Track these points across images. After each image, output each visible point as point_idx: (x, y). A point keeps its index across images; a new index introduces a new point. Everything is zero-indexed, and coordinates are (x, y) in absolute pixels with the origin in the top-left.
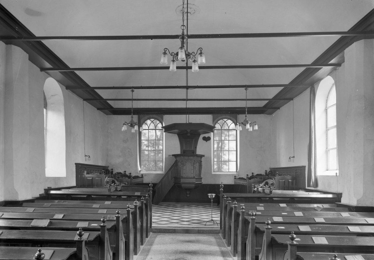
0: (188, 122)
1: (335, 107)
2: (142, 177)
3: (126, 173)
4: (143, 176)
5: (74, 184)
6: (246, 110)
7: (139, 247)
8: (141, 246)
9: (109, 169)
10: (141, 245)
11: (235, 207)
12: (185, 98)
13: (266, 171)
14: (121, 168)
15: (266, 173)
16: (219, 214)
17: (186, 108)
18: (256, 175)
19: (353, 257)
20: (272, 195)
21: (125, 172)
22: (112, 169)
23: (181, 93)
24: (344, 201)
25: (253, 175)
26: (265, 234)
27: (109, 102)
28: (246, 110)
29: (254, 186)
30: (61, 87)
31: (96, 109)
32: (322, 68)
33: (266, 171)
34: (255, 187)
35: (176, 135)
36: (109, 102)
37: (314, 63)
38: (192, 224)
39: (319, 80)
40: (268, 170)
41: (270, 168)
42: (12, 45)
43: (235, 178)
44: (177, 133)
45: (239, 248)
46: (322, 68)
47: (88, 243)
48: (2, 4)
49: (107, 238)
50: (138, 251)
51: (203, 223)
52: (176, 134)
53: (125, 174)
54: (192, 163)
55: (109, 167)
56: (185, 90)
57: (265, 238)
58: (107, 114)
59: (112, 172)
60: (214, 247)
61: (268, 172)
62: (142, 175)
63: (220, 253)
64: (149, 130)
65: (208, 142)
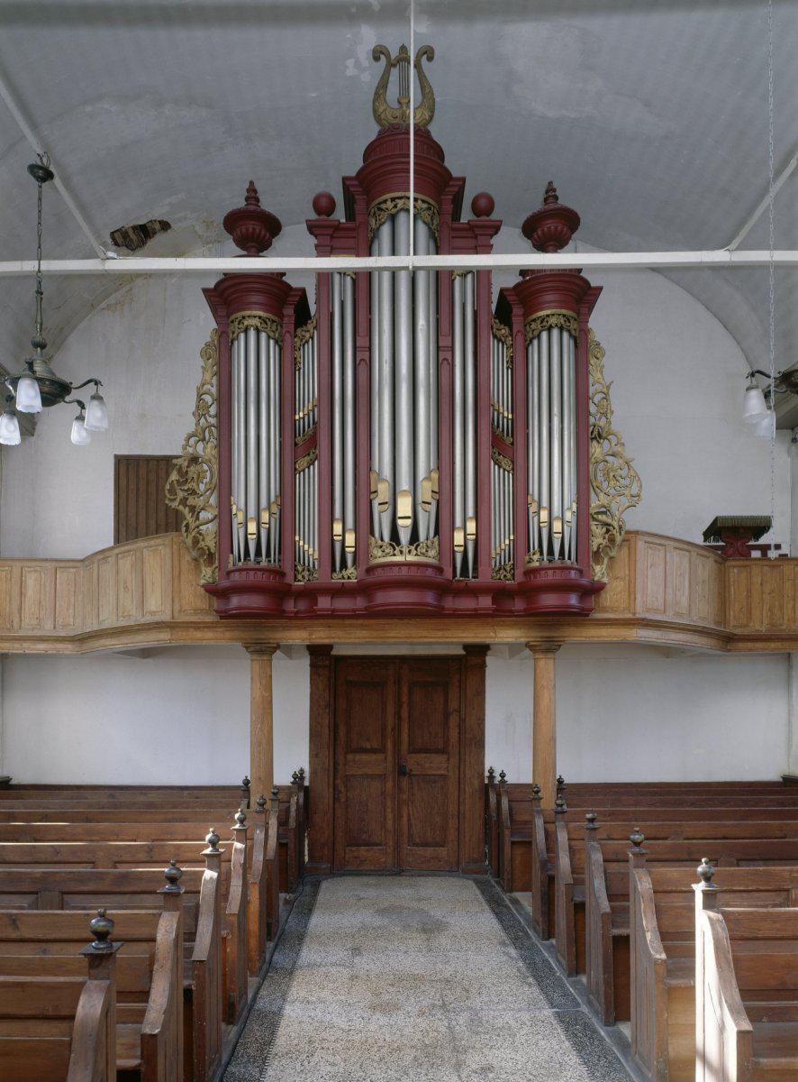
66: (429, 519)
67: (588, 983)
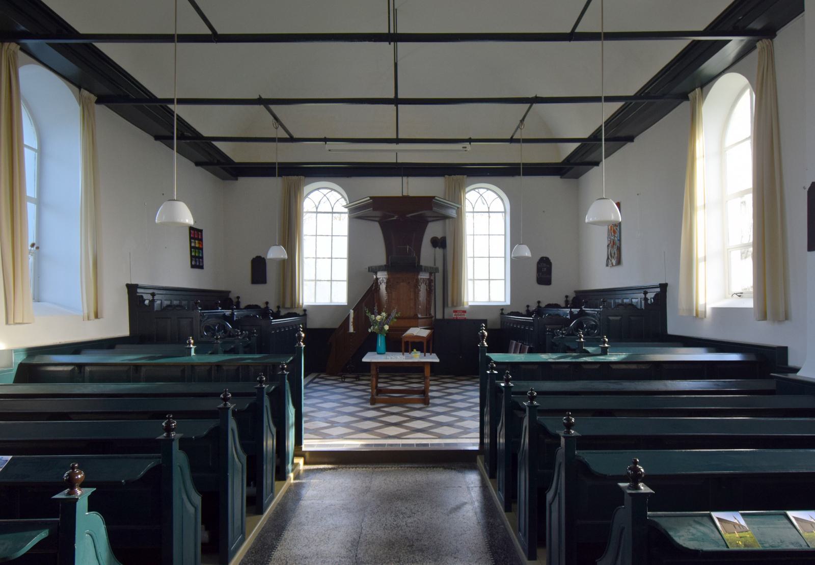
0: (405, 179)
3: (269, 306)
4: (307, 313)
5: (125, 331)
6: (521, 167)
9: (233, 296)
11: (532, 407)
13: (567, 297)
16: (478, 382)
17: (397, 164)
18: (545, 307)
19: (378, 217)
21: (267, 303)
22: (238, 298)
25: (539, 307)
27: (217, 144)
28: (521, 167)
30: (68, 86)
31: (193, 164)
32: (729, 41)
33: (567, 297)
36: (218, 144)
37: (709, 31)
39: (708, 81)
40: (572, 295)
41: (576, 292)
43: (502, 314)
44: (377, 219)
46: (729, 41)
50: (265, 502)
51: (445, 394)
52: (376, 221)
53: (267, 308)
58: (224, 178)
61: (570, 299)
62: (305, 310)
64: (334, 215)
65: (635, 140)
66: (764, 222)
67: (269, 107)
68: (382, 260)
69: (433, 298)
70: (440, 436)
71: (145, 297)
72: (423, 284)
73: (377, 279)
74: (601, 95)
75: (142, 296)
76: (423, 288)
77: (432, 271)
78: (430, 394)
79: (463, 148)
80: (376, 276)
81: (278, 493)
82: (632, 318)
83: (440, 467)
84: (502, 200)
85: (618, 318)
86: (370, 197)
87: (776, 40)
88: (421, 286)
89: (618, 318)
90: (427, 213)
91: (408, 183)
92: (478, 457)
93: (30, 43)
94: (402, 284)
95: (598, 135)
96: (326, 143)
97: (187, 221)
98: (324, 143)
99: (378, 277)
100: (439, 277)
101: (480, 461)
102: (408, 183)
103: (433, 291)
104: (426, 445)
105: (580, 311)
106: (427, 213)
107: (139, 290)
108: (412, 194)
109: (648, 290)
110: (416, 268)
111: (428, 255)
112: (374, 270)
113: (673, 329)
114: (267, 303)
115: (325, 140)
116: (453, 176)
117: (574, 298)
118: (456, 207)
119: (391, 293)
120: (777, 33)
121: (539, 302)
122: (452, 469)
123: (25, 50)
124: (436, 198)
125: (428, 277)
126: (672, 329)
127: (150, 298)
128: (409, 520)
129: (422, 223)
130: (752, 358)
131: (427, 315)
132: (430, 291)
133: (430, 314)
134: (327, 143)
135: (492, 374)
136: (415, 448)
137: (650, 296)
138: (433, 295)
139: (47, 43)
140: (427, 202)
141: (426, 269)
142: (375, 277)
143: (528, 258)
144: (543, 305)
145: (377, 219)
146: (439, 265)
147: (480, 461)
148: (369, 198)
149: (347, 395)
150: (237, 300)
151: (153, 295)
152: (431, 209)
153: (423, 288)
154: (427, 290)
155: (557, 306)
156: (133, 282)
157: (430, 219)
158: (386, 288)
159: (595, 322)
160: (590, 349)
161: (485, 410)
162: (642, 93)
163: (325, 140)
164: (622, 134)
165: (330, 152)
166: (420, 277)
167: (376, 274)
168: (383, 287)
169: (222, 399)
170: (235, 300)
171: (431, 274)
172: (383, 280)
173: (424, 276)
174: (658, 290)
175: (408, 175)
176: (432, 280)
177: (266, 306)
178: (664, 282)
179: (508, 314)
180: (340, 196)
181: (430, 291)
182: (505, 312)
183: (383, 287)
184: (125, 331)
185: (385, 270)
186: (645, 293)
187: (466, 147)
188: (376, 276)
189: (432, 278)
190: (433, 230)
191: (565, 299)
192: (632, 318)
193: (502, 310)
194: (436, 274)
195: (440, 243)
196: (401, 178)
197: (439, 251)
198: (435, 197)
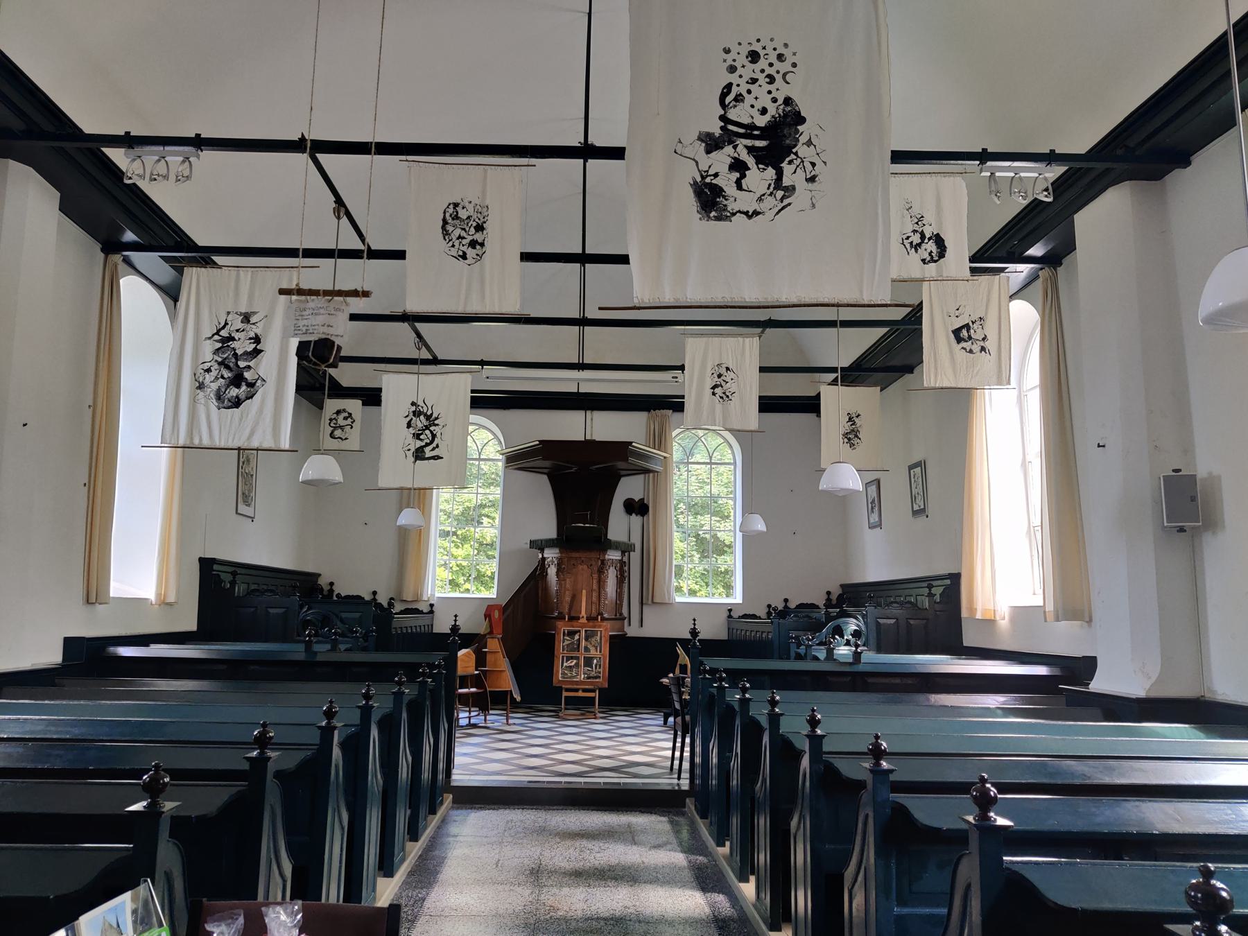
0: (589, 413)
1: (1037, 391)
2: (431, 612)
5: (192, 626)
7: (403, 849)
8: (409, 845)
9: (323, 582)
10: (410, 841)
12: (575, 314)
13: (829, 593)
14: (475, 874)
15: (829, 600)
17: (578, 394)
18: (795, 608)
20: (860, 668)
21: (375, 593)
22: (332, 584)
23: (561, 345)
24: (1098, 685)
25: (786, 607)
26: (865, 796)
29: (797, 638)
30: (162, 297)
33: (829, 593)
34: (799, 645)
35: (545, 477)
38: (591, 772)
40: (836, 592)
41: (842, 586)
42: (11, 161)
43: (730, 616)
44: (546, 471)
45: (763, 858)
47: (180, 825)
48: (2, 49)
49: (272, 807)
50: (396, 860)
53: (375, 599)
54: (596, 569)
55: (320, 575)
56: (597, 140)
57: (867, 811)
59: (331, 591)
60: (668, 852)
61: (834, 597)
63: (687, 875)
68: (551, 532)
69: (626, 590)
70: (636, 776)
71: (223, 576)
72: (611, 568)
73: (544, 559)
74: (841, 329)
75: (218, 575)
76: (611, 576)
77: (626, 549)
78: (647, 475)
79: (673, 377)
80: (543, 555)
81: (409, 855)
82: (912, 622)
83: (636, 811)
84: (731, 447)
85: (892, 621)
86: (539, 441)
87: (1060, 269)
88: (609, 571)
89: (892, 621)
90: (621, 465)
91: (592, 419)
92: (688, 800)
93: (134, 256)
94: (580, 567)
95: (862, 363)
96: (482, 368)
97: (337, 478)
98: (480, 367)
99: (545, 556)
100: (635, 557)
101: (690, 802)
102: (592, 419)
103: (627, 581)
104: (619, 784)
105: (839, 611)
106: (621, 465)
107: (215, 567)
108: (599, 437)
109: (934, 583)
110: (602, 543)
111: (619, 526)
112: (539, 545)
113: (969, 640)
114: (375, 593)
115: (482, 363)
116: (662, 411)
117: (840, 595)
118: (662, 456)
119: (565, 580)
120: (1063, 261)
121: (786, 600)
122: (651, 813)
123: (127, 261)
124: (634, 444)
125: (620, 558)
126: (967, 642)
127: (230, 578)
128: (598, 855)
129: (610, 482)
130: (1055, 671)
131: (616, 616)
132: (622, 578)
133: (621, 614)
134: (485, 367)
135: (705, 678)
136: (602, 787)
137: (937, 591)
138: (627, 585)
139: (160, 256)
140: (621, 450)
141: (616, 546)
142: (540, 556)
143: (760, 533)
144: (792, 605)
145: (546, 471)
146: (636, 540)
147: (690, 802)
148: (538, 443)
149: (489, 747)
150: (329, 587)
151: (234, 574)
152: (626, 460)
153: (611, 576)
154: (617, 577)
155: (813, 606)
156: (208, 556)
157: (623, 473)
158: (557, 574)
159: (858, 626)
160: (186, 244)
161: (696, 730)
162: (913, 316)
163: (482, 363)
164: (896, 362)
165: (488, 380)
166: (607, 557)
167: (542, 551)
168: (552, 571)
169: (396, 682)
170: (326, 588)
171: (623, 553)
172: (553, 562)
173: (614, 555)
174: (948, 582)
175: (593, 409)
176: (625, 562)
177: (373, 597)
178: (956, 572)
179: (739, 617)
180: (491, 437)
181: (622, 578)
182: (735, 615)
183: (552, 571)
184: (192, 626)
185: (557, 547)
186: (930, 587)
187: (677, 378)
188: (543, 555)
189: (625, 559)
190: (628, 488)
191: (826, 597)
192: (912, 622)
193: (730, 610)
194: (632, 553)
195: (637, 508)
196: (584, 412)
197: (636, 520)
198: (632, 442)
